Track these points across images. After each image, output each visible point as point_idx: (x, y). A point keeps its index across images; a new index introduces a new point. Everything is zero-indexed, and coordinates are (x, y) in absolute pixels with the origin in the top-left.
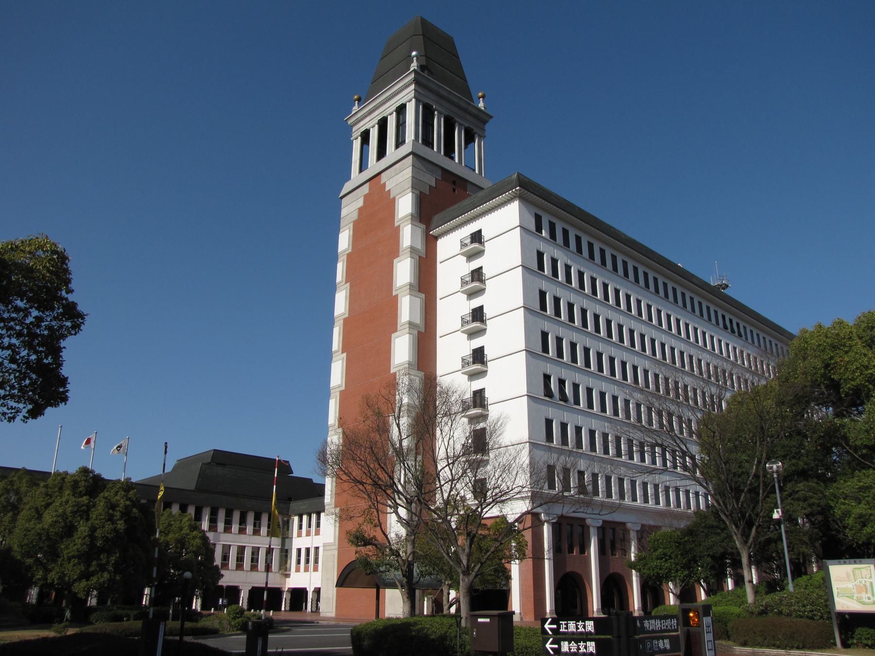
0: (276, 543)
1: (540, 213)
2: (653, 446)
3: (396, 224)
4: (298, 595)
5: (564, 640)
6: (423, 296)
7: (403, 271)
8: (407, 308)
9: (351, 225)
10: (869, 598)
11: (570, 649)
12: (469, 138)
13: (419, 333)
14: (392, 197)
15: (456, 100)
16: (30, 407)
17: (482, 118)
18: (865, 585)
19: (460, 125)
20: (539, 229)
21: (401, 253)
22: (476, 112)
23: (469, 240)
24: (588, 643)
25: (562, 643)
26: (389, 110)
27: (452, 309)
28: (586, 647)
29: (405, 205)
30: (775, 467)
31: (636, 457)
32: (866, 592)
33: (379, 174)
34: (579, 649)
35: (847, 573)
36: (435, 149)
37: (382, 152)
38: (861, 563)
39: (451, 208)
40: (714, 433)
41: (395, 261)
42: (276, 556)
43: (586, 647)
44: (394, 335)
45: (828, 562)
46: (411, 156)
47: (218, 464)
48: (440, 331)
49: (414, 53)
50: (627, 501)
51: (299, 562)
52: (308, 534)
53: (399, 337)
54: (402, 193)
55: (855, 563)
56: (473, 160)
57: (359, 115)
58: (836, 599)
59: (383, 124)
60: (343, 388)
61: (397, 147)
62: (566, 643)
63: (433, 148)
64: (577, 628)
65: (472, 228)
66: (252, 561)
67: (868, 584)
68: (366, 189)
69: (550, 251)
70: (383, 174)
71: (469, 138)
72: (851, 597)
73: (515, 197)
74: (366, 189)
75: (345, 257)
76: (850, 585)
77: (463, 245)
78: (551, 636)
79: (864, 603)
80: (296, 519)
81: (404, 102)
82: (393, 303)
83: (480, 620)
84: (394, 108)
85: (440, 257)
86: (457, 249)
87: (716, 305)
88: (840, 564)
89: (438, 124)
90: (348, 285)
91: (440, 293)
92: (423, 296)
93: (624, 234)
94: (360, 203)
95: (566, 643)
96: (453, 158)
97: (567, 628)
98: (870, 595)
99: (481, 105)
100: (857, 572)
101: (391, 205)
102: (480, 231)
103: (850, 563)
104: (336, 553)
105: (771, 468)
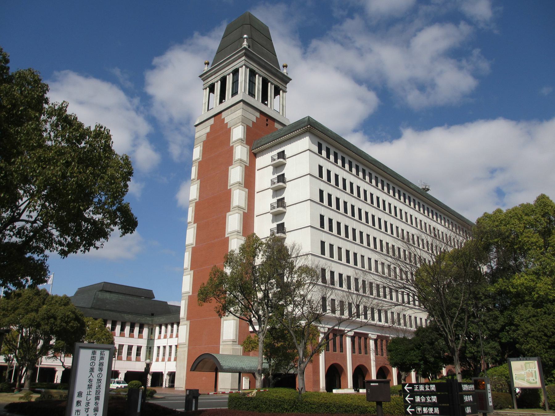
0: (143, 343)
1: (321, 142)
3: (231, 145)
4: (158, 377)
5: (417, 395)
7: (236, 174)
8: (238, 197)
9: (202, 144)
10: (534, 380)
11: (421, 400)
14: (228, 127)
16: (489, 271)
18: (532, 373)
19: (272, 84)
20: (320, 152)
21: (233, 163)
22: (281, 76)
23: (277, 157)
24: (432, 397)
25: (416, 397)
28: (431, 399)
31: (388, 297)
32: (532, 376)
33: (220, 113)
34: (426, 400)
35: (522, 366)
36: (256, 98)
37: (222, 97)
38: (530, 360)
41: (230, 168)
42: (143, 352)
43: (431, 399)
44: (228, 214)
45: (511, 359)
46: (242, 103)
47: (106, 291)
48: (256, 213)
49: (245, 36)
51: (158, 355)
52: (165, 337)
53: (231, 215)
54: (236, 125)
55: (526, 360)
58: (515, 380)
60: (194, 245)
61: (232, 96)
62: (418, 397)
63: (255, 98)
64: (425, 389)
66: (137, 355)
67: (533, 372)
68: (212, 121)
69: (327, 165)
70: (223, 113)
72: (524, 380)
74: (212, 121)
75: (197, 164)
76: (523, 373)
77: (273, 160)
78: (409, 393)
79: (531, 383)
80: (157, 329)
82: (228, 195)
83: (372, 384)
84: (231, 70)
85: (257, 167)
86: (269, 162)
87: (433, 207)
88: (517, 360)
89: (258, 81)
90: (199, 181)
91: (257, 190)
92: (247, 190)
94: (208, 130)
95: (418, 397)
96: (267, 105)
97: (419, 389)
98: (534, 378)
100: (528, 365)
101: (228, 132)
102: (283, 152)
103: (523, 360)
104: (186, 349)
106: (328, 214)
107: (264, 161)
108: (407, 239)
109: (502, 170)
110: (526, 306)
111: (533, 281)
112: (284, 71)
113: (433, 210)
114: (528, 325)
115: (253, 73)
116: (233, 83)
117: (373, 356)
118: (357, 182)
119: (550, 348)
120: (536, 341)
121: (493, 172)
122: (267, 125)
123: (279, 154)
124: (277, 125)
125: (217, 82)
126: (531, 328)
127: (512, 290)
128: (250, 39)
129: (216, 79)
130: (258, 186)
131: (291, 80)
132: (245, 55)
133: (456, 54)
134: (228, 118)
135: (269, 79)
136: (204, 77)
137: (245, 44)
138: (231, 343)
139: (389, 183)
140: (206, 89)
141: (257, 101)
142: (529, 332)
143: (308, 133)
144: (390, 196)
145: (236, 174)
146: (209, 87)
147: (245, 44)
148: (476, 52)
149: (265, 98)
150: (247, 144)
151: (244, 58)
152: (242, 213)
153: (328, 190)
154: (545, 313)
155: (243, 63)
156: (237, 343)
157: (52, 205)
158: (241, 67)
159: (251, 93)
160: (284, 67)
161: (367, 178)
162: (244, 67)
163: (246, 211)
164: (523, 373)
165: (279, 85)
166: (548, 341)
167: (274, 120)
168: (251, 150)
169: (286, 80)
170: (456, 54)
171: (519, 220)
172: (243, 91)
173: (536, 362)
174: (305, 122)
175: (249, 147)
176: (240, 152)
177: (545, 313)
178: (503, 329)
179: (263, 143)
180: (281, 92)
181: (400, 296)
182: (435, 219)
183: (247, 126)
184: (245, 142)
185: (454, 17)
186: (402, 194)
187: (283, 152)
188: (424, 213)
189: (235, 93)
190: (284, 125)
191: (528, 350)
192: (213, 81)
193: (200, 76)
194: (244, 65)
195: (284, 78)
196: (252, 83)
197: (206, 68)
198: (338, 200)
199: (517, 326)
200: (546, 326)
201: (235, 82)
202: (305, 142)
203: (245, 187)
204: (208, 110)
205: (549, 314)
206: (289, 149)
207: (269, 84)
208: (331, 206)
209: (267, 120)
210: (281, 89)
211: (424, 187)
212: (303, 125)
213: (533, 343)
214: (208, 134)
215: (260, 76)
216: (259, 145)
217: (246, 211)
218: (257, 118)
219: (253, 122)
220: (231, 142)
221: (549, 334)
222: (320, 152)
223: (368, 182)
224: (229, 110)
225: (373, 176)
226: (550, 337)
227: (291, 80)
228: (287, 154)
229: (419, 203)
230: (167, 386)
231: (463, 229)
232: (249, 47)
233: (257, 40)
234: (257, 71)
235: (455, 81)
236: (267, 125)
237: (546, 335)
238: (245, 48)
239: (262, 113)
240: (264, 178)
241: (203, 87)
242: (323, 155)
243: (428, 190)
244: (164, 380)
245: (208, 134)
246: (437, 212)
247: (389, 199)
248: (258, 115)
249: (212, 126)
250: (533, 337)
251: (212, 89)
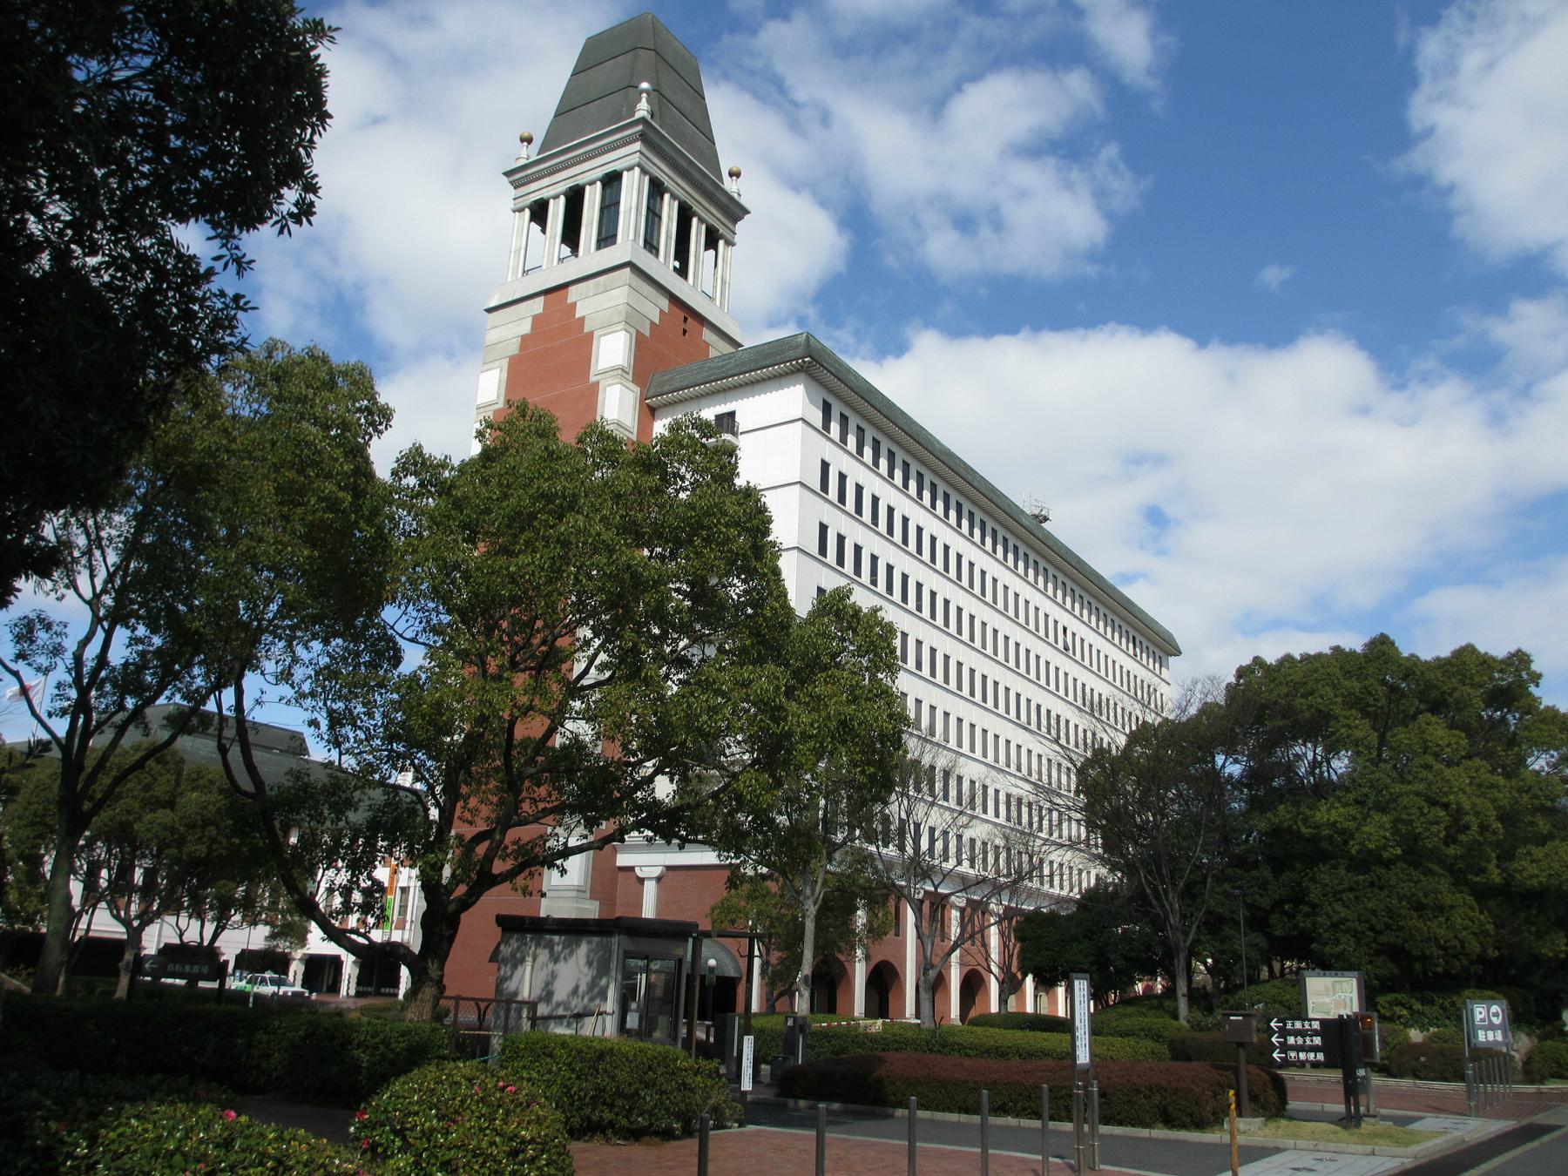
1: (831, 400)
2: (1050, 811)
3: (593, 379)
9: (505, 363)
12: (712, 240)
15: (699, 178)
19: (701, 220)
20: (826, 427)
22: (725, 200)
26: (590, 172)
39: (1319, 644)
40: (171, 805)
49: (645, 85)
50: (1046, 887)
54: (608, 327)
59: (575, 198)
63: (657, 255)
68: (538, 305)
69: (841, 462)
70: (572, 289)
71: (712, 240)
74: (538, 305)
76: (1328, 1000)
84: (600, 173)
94: (526, 327)
101: (583, 344)
102: (732, 414)
108: (1093, 707)
109: (1159, 460)
110: (1335, 867)
111: (1354, 819)
112: (730, 185)
113: (1019, 544)
114: (1339, 908)
116: (602, 209)
117: (995, 955)
118: (918, 516)
119: (1377, 953)
120: (1352, 940)
121: (1138, 460)
122: (685, 332)
123: (719, 417)
124: (707, 335)
126: (1344, 912)
127: (1304, 830)
128: (657, 93)
129: (553, 189)
131: (748, 212)
132: (643, 137)
133: (1064, 148)
134: (588, 304)
135: (696, 208)
136: (517, 176)
137: (643, 109)
138: (574, 894)
139: (879, 437)
140: (521, 210)
141: (662, 266)
142: (1343, 921)
143: (802, 376)
144: (909, 496)
147: (643, 109)
148: (1111, 151)
150: (634, 381)
151: (637, 146)
154: (1372, 884)
155: (636, 159)
156: (588, 895)
158: (630, 169)
159: (651, 245)
160: (731, 175)
161: (868, 452)
162: (637, 170)
164: (1328, 1000)
166: (1375, 941)
167: (702, 320)
168: (643, 398)
169: (735, 211)
170: (1064, 148)
171: (1334, 686)
172: (631, 236)
173: (1354, 981)
174: (797, 347)
177: (1372, 884)
178: (1278, 905)
179: (677, 385)
180: (721, 243)
181: (1074, 833)
182: (1021, 570)
183: (638, 332)
184: (630, 377)
185: (1063, 49)
186: (927, 484)
187: (732, 414)
188: (983, 542)
189: (607, 238)
190: (736, 344)
191: (1338, 956)
192: (544, 194)
193: (508, 174)
194: (639, 165)
195: (732, 207)
196: (653, 215)
197: (528, 153)
199: (1313, 906)
200: (1374, 912)
201: (610, 208)
202: (794, 399)
204: (525, 272)
205: (1381, 888)
207: (695, 220)
209: (685, 320)
210: (722, 237)
211: (1036, 512)
212: (792, 354)
213: (1347, 944)
214: (524, 339)
215: (674, 197)
216: (666, 389)
218: (662, 312)
219: (652, 323)
220: (593, 371)
221: (1378, 927)
223: (854, 451)
224: (591, 282)
225: (835, 414)
226: (1380, 933)
227: (748, 212)
228: (742, 421)
229: (971, 515)
230: (352, 992)
231: (1016, 548)
233: (669, 95)
234: (667, 182)
235: (1059, 218)
236: (685, 332)
237: (1372, 929)
238: (643, 120)
239: (675, 300)
241: (511, 205)
243: (1046, 519)
244: (345, 977)
245: (524, 338)
246: (974, 510)
247: (890, 496)
248: (664, 303)
249: (537, 320)
250: (1347, 931)
251: (539, 212)
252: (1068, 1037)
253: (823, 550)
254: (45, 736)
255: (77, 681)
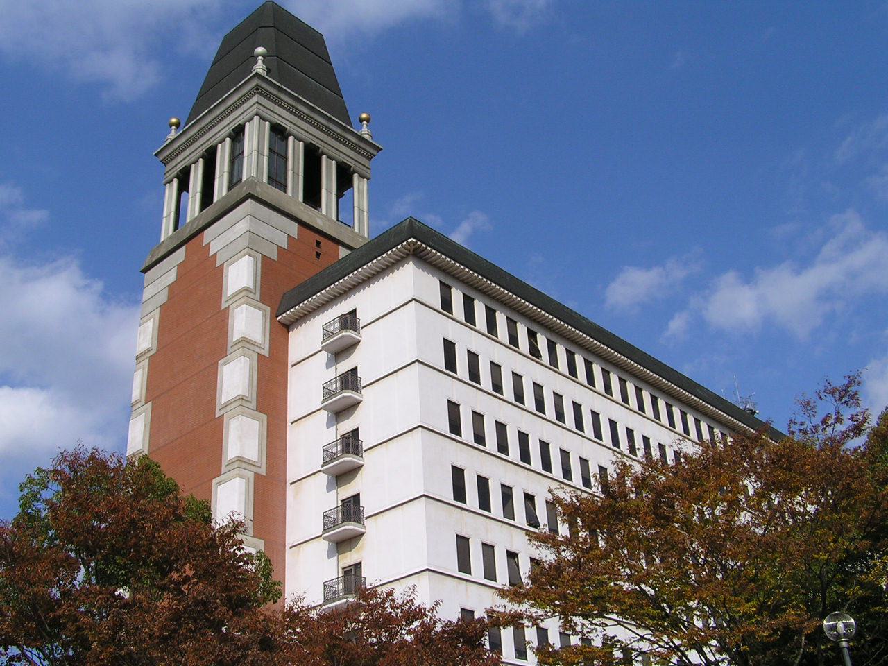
6: (265, 417)
7: (235, 378)
8: (242, 438)
13: (257, 476)
17: (368, 149)
19: (330, 157)
21: (229, 350)
23: (338, 325)
27: (309, 441)
29: (240, 275)
30: (840, 625)
46: (250, 200)
48: (291, 475)
49: (260, 50)
54: (233, 258)
56: (359, 215)
57: (176, 145)
65: (343, 308)
69: (466, 341)
71: (345, 179)
73: (407, 255)
74: (180, 255)
81: (240, 121)
85: (293, 357)
89: (295, 154)
93: (586, 320)
94: (172, 277)
99: (364, 131)
101: (216, 275)
105: (834, 628)
106: (475, 464)
107: (307, 339)
115: (279, 132)
122: (318, 255)
125: (196, 162)
129: (192, 157)
130: (295, 408)
137: (259, 67)
145: (235, 378)
146: (177, 177)
147: (259, 67)
149: (312, 196)
151: (255, 99)
152: (251, 475)
153: (470, 400)
157: (98, 587)
162: (256, 118)
163: (263, 471)
165: (315, 142)
175: (268, 309)
176: (247, 322)
184: (258, 297)
196: (278, 157)
198: (544, 446)
203: (260, 409)
206: (366, 302)
208: (550, 471)
209: (318, 243)
215: (297, 138)
217: (263, 471)
220: (224, 299)
222: (447, 305)
228: (362, 317)
232: (269, 71)
236: (318, 255)
240: (308, 382)
242: (478, 327)
248: (293, 228)
252: (476, 433)
253: (464, 565)
254: (671, 437)
255: (700, 445)
